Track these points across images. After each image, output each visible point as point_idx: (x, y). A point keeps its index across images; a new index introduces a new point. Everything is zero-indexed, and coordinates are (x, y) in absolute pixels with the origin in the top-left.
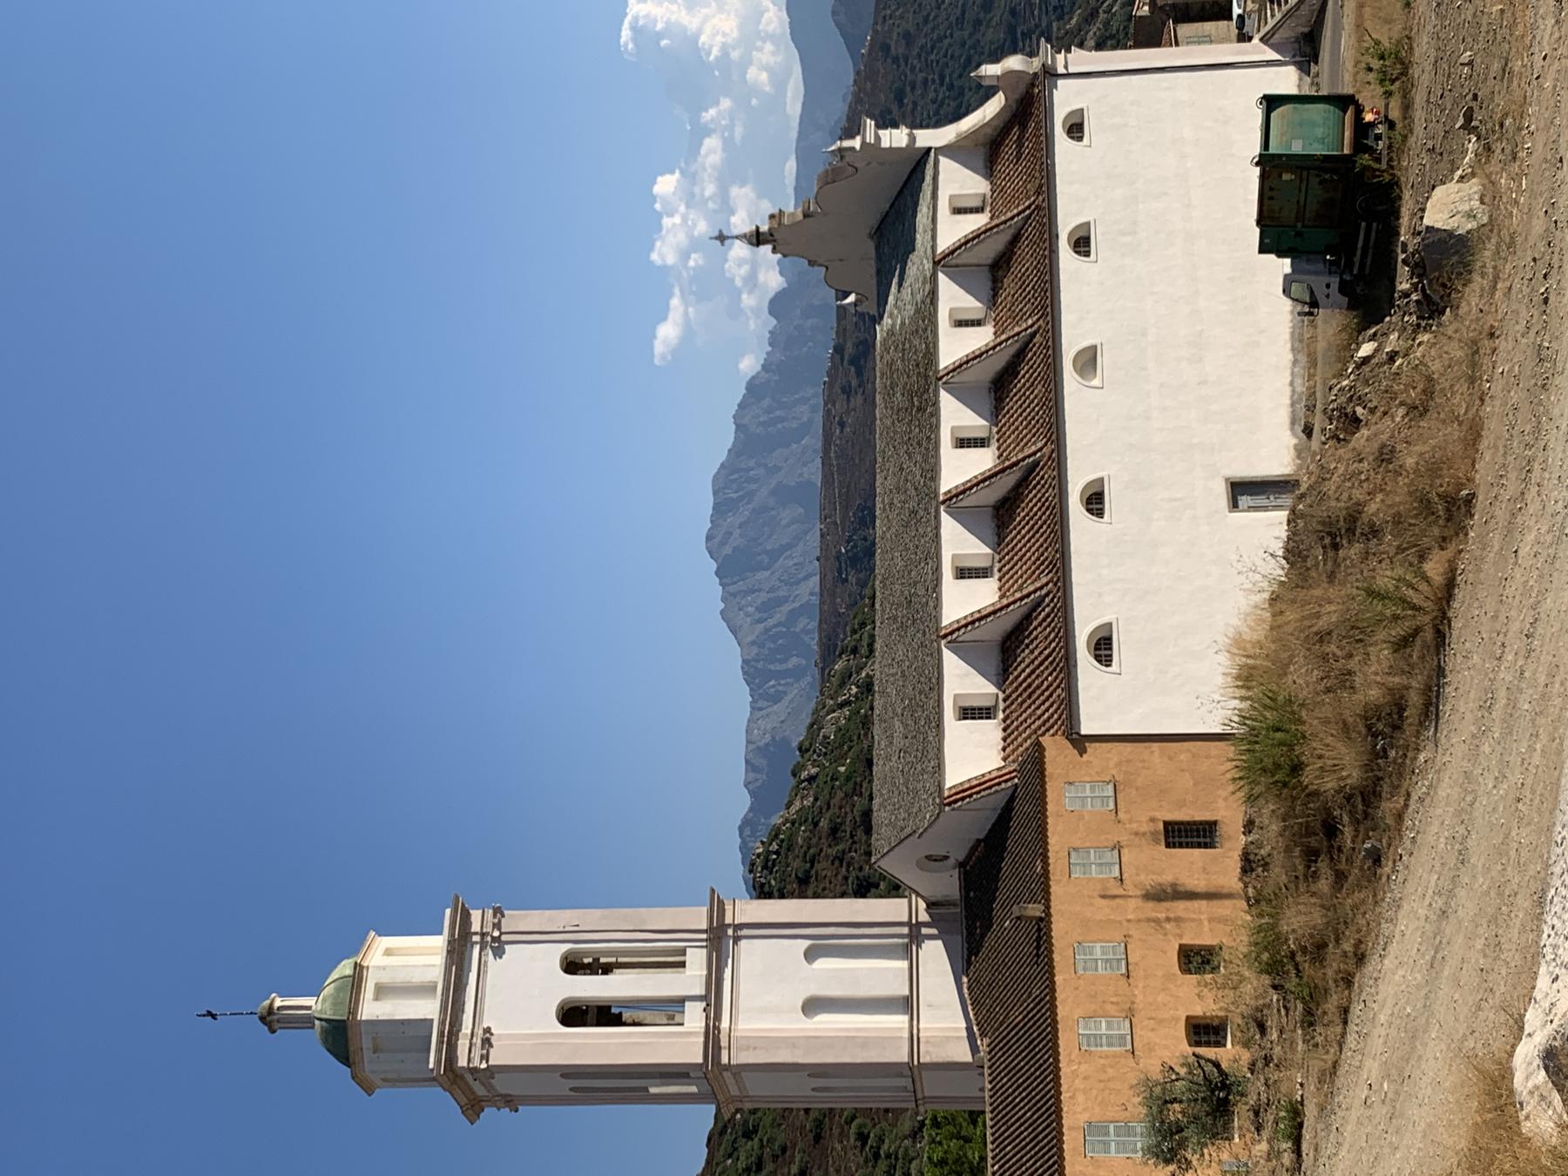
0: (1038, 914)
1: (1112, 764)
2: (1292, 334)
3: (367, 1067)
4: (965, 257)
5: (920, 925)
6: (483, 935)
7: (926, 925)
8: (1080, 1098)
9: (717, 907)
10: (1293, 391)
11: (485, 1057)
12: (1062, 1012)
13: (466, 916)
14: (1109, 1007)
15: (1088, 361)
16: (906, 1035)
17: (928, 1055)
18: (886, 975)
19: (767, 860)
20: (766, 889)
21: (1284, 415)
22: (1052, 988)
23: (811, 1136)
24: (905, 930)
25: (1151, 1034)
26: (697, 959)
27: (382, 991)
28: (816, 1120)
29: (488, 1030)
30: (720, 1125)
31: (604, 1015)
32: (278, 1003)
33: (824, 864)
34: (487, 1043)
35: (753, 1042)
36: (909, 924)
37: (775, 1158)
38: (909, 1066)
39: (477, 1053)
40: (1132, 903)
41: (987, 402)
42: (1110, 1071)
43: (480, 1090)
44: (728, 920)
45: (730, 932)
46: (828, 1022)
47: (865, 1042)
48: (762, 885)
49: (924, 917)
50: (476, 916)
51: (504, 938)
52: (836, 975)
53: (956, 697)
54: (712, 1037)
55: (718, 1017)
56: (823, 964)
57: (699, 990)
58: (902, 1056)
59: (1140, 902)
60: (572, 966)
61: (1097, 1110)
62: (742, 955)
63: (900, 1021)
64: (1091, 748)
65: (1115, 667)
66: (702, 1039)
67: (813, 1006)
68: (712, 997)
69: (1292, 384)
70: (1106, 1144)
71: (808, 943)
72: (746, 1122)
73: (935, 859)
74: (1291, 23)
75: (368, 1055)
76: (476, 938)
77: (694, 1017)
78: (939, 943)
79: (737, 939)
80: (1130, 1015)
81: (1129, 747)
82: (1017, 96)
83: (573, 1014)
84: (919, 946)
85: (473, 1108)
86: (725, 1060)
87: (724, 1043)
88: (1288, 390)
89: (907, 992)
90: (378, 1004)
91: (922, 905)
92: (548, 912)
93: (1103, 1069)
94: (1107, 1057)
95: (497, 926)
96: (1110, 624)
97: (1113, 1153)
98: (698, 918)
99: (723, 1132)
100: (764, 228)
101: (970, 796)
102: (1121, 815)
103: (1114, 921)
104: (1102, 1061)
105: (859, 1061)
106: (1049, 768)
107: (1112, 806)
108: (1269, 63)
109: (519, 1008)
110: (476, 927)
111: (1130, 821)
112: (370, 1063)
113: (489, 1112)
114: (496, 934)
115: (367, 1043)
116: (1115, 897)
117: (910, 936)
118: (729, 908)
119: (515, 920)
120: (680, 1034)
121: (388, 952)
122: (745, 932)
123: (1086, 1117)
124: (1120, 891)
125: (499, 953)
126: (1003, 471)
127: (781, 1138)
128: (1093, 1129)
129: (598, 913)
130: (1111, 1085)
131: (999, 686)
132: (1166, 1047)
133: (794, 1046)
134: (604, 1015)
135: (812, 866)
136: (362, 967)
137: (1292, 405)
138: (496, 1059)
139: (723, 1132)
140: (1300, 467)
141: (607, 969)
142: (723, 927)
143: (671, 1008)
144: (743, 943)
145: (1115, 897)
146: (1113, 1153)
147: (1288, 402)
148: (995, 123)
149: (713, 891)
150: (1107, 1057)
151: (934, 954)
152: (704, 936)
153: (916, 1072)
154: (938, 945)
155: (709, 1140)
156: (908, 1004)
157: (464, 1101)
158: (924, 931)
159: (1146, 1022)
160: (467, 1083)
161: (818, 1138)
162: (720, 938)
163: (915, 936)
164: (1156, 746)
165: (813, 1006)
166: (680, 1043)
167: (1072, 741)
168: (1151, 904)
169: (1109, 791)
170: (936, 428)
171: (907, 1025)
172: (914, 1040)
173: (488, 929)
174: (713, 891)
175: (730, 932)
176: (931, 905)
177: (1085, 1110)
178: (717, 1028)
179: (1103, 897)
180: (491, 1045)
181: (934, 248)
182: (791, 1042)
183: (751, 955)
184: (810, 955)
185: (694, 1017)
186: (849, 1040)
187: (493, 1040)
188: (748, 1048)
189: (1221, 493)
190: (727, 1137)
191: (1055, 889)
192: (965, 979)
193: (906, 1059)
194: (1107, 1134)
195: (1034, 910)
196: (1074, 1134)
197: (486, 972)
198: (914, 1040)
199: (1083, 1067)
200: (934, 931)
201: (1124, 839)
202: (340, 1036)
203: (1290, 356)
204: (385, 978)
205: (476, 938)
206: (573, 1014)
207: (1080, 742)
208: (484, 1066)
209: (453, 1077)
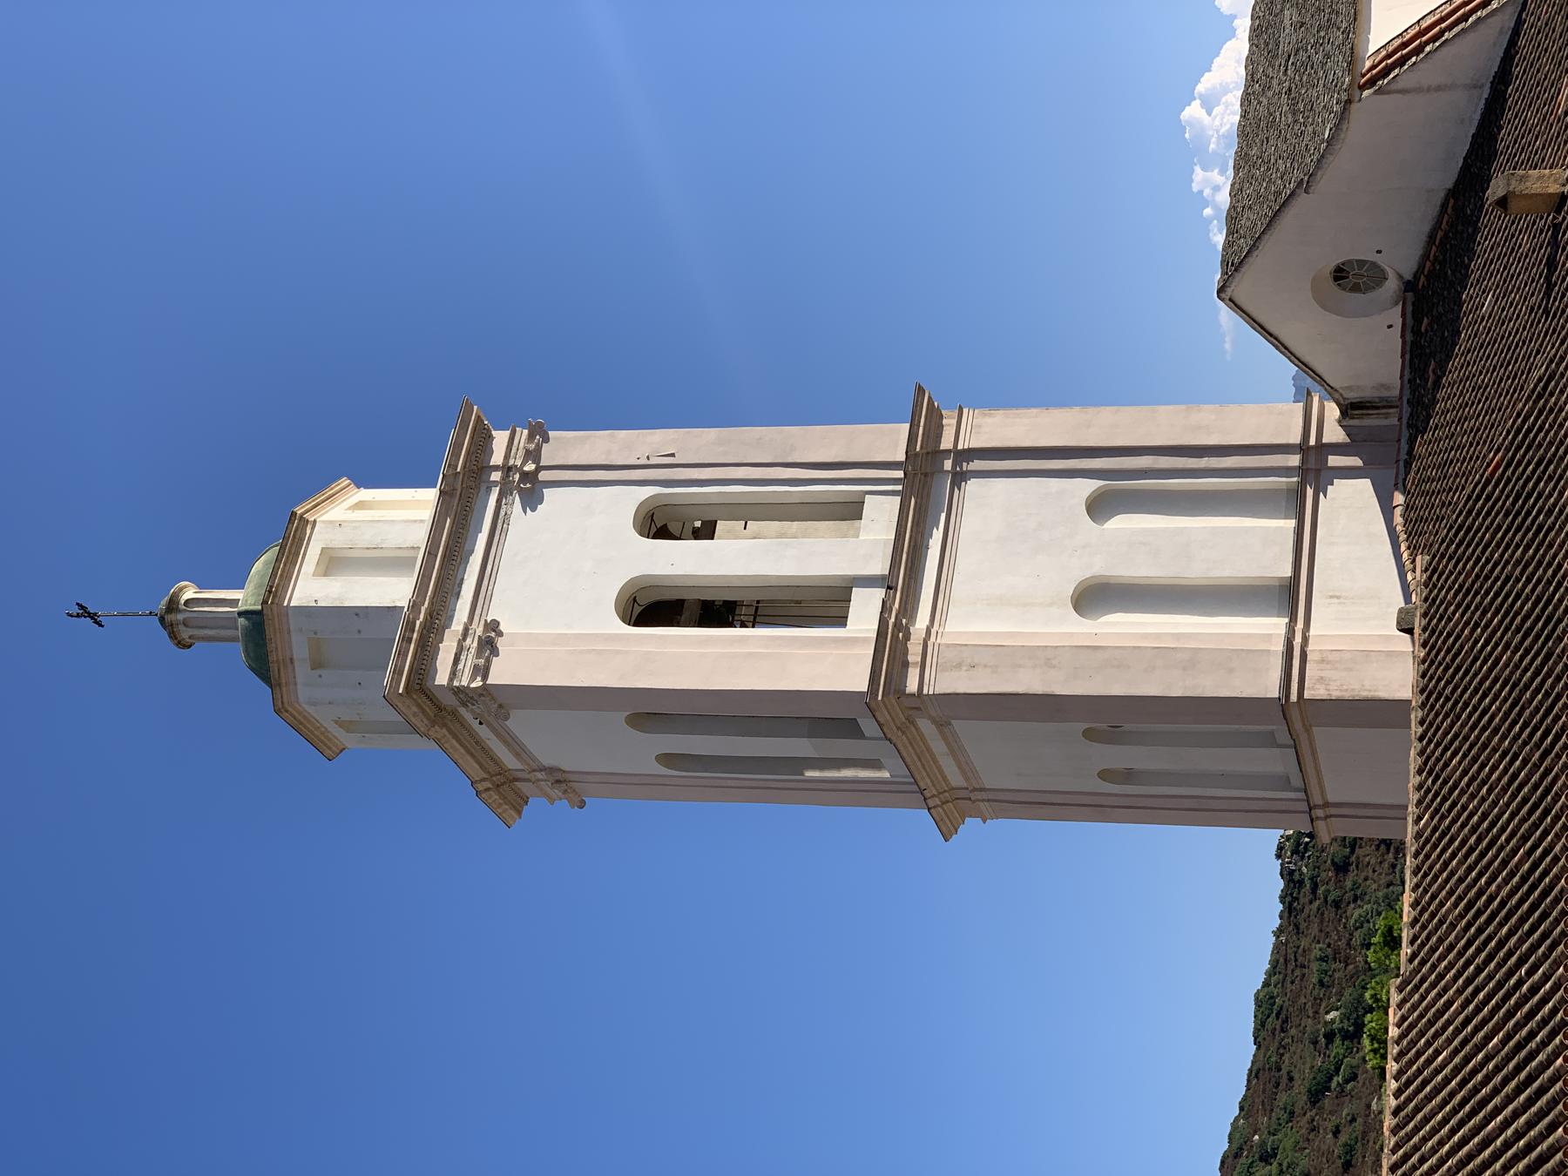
5: (1325, 449)
6: (507, 469)
7: (1337, 449)
9: (926, 420)
11: (484, 671)
13: (483, 440)
16: (1279, 647)
18: (1254, 544)
19: (1299, 844)
20: (1296, 877)
23: (1339, 1163)
24: (1294, 460)
26: (882, 514)
27: (333, 563)
28: (1346, 1145)
29: (493, 626)
30: (1235, 1146)
31: (716, 610)
32: (189, 594)
33: (1368, 850)
34: (489, 646)
35: (971, 655)
36: (1303, 448)
38: (1282, 706)
39: (469, 661)
43: (483, 737)
44: (946, 443)
46: (1121, 626)
47: (1192, 658)
48: (1291, 872)
49: (1334, 433)
50: (500, 438)
54: (891, 646)
56: (1121, 523)
58: (1268, 686)
60: (658, 524)
67: (1094, 596)
71: (1091, 485)
72: (1263, 1143)
75: (302, 671)
76: (496, 476)
77: (865, 610)
78: (1366, 484)
79: (959, 478)
83: (653, 607)
84: (1320, 489)
86: (912, 686)
87: (914, 655)
89: (1287, 572)
91: (1333, 411)
92: (622, 434)
95: (533, 455)
98: (891, 441)
99: (1237, 1156)
101: (1417, 51)
109: (558, 593)
110: (497, 458)
112: (307, 689)
113: (536, 806)
114: (530, 467)
115: (300, 649)
118: (949, 423)
119: (565, 446)
120: (836, 640)
121: (360, 505)
122: (977, 465)
125: (532, 500)
129: (712, 433)
133: (1049, 663)
134: (716, 610)
135: (1353, 852)
138: (503, 672)
139: (1237, 1156)
142: (937, 455)
144: (972, 486)
149: (920, 391)
151: (1354, 514)
152: (900, 474)
153: (1295, 715)
154: (1362, 489)
155: (1223, 1162)
156: (1289, 596)
157: (478, 773)
158: (1334, 461)
160: (472, 734)
163: (1314, 467)
165: (1094, 596)
166: (832, 662)
171: (1283, 631)
172: (1293, 656)
174: (920, 391)
175: (948, 465)
176: (1350, 409)
178: (903, 630)
180: (495, 652)
182: (1045, 656)
183: (984, 505)
184: (1099, 508)
185: (865, 610)
186: (1161, 654)
187: (501, 643)
188: (959, 666)
190: (1243, 1160)
193: (1274, 692)
197: (504, 531)
198: (1293, 656)
200: (1355, 461)
202: (260, 633)
204: (338, 540)
205: (496, 476)
206: (653, 607)
208: (478, 683)
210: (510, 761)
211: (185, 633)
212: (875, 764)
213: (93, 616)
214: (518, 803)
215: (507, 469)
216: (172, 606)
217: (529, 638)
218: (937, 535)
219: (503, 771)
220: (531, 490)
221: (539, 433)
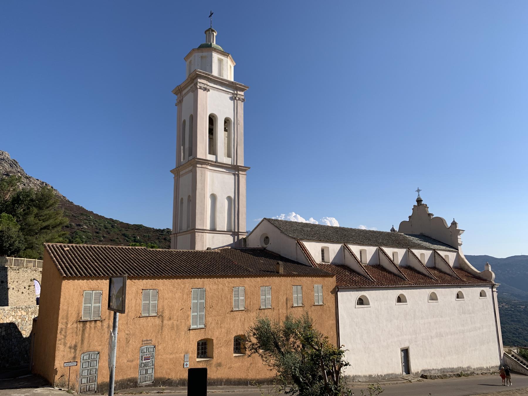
0: (280, 271)
1: (329, 304)
2: (444, 369)
3: (196, 54)
4: (438, 259)
5: (238, 235)
6: (237, 94)
8: (215, 287)
10: (431, 370)
11: (200, 88)
12: (247, 280)
13: (242, 90)
14: (249, 300)
15: (433, 297)
16: (205, 228)
17: (198, 235)
18: (222, 224)
21: (426, 367)
22: (256, 276)
24: (236, 231)
25: (239, 318)
26: (228, 161)
27: (220, 61)
29: (209, 90)
32: (215, 34)
34: (205, 89)
36: (238, 232)
37: (107, 231)
38: (194, 229)
39: (202, 86)
40: (284, 311)
41: (404, 264)
42: (225, 301)
44: (240, 172)
45: (237, 172)
49: (241, 237)
50: (242, 93)
51: (236, 101)
52: (223, 206)
53: (328, 248)
54: (205, 162)
55: (212, 165)
56: (226, 202)
57: (219, 160)
59: (285, 315)
60: (227, 121)
61: (210, 294)
62: (230, 176)
63: (208, 228)
64: (333, 296)
65: (357, 306)
66: (204, 158)
67: (214, 197)
68: (217, 164)
69: (433, 369)
70: (197, 299)
71: (233, 197)
73: (266, 239)
74: (513, 363)
76: (236, 92)
79: (234, 174)
80: (246, 310)
81: (334, 311)
82: (481, 276)
83: (212, 120)
84: (231, 235)
85: (179, 91)
86: (198, 166)
87: (203, 166)
88: (431, 368)
89: (217, 230)
90: (217, 59)
91: (244, 237)
93: (226, 297)
94: (230, 299)
95: (239, 99)
96: (369, 304)
97: (193, 301)
100: (423, 203)
102: (313, 307)
103: (278, 304)
104: (229, 297)
105: (197, 211)
106: (327, 279)
107: (316, 304)
108: (500, 356)
109: (213, 102)
110: (239, 92)
111: (311, 311)
112: (197, 55)
114: (237, 98)
115: (204, 54)
116: (287, 304)
117: (235, 232)
118: (244, 173)
119: (241, 105)
122: (236, 177)
123: (208, 289)
124: (289, 306)
125: (231, 99)
126: (397, 267)
127: (111, 233)
128: (203, 293)
129: (242, 131)
130: (220, 301)
131: (332, 263)
132: (234, 327)
136: (228, 56)
137: (428, 370)
138: (200, 92)
140: (413, 374)
141: (225, 130)
143: (212, 150)
144: (233, 177)
145: (287, 304)
146: (193, 301)
147: (429, 368)
148: (469, 269)
149: (249, 168)
150: (230, 299)
151: (227, 240)
156: (213, 230)
157: (182, 86)
158: (236, 237)
159: (243, 317)
161: (111, 240)
162: (234, 169)
163: (235, 234)
164: (335, 322)
165: (214, 197)
166: (202, 151)
167: (334, 289)
168: (284, 320)
169: (321, 303)
170: (397, 247)
172: (203, 231)
173: (238, 96)
174: (249, 168)
175: (237, 172)
176: (245, 240)
177: (210, 289)
178: (208, 164)
179: (287, 299)
180: (204, 90)
181: (438, 249)
182: (203, 189)
183: (230, 179)
184: (229, 198)
189: (404, 346)
191: (289, 279)
192: (230, 248)
193: (196, 227)
194: (201, 299)
195: (281, 271)
196: (201, 283)
198: (203, 231)
199: (226, 289)
200: (236, 241)
201: (305, 309)
202: (207, 47)
203: (440, 368)
204: (224, 62)
205: (236, 92)
206: (212, 120)
207: (335, 292)
208: (198, 87)
209: (193, 78)
210: (184, 92)
211: (207, 33)
212: (184, 159)
213: (211, 16)
214: (176, 93)
215: (237, 94)
216: (213, 31)
217: (206, 97)
218: (225, 170)
219: (182, 91)
220: (233, 99)
221: (243, 100)
